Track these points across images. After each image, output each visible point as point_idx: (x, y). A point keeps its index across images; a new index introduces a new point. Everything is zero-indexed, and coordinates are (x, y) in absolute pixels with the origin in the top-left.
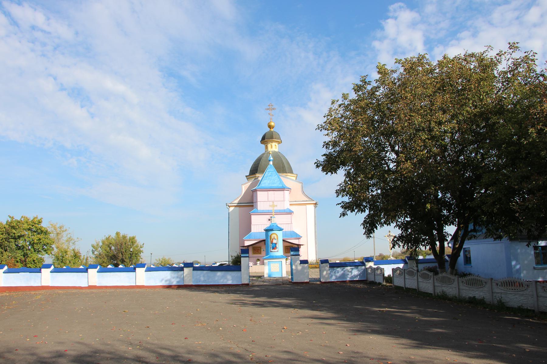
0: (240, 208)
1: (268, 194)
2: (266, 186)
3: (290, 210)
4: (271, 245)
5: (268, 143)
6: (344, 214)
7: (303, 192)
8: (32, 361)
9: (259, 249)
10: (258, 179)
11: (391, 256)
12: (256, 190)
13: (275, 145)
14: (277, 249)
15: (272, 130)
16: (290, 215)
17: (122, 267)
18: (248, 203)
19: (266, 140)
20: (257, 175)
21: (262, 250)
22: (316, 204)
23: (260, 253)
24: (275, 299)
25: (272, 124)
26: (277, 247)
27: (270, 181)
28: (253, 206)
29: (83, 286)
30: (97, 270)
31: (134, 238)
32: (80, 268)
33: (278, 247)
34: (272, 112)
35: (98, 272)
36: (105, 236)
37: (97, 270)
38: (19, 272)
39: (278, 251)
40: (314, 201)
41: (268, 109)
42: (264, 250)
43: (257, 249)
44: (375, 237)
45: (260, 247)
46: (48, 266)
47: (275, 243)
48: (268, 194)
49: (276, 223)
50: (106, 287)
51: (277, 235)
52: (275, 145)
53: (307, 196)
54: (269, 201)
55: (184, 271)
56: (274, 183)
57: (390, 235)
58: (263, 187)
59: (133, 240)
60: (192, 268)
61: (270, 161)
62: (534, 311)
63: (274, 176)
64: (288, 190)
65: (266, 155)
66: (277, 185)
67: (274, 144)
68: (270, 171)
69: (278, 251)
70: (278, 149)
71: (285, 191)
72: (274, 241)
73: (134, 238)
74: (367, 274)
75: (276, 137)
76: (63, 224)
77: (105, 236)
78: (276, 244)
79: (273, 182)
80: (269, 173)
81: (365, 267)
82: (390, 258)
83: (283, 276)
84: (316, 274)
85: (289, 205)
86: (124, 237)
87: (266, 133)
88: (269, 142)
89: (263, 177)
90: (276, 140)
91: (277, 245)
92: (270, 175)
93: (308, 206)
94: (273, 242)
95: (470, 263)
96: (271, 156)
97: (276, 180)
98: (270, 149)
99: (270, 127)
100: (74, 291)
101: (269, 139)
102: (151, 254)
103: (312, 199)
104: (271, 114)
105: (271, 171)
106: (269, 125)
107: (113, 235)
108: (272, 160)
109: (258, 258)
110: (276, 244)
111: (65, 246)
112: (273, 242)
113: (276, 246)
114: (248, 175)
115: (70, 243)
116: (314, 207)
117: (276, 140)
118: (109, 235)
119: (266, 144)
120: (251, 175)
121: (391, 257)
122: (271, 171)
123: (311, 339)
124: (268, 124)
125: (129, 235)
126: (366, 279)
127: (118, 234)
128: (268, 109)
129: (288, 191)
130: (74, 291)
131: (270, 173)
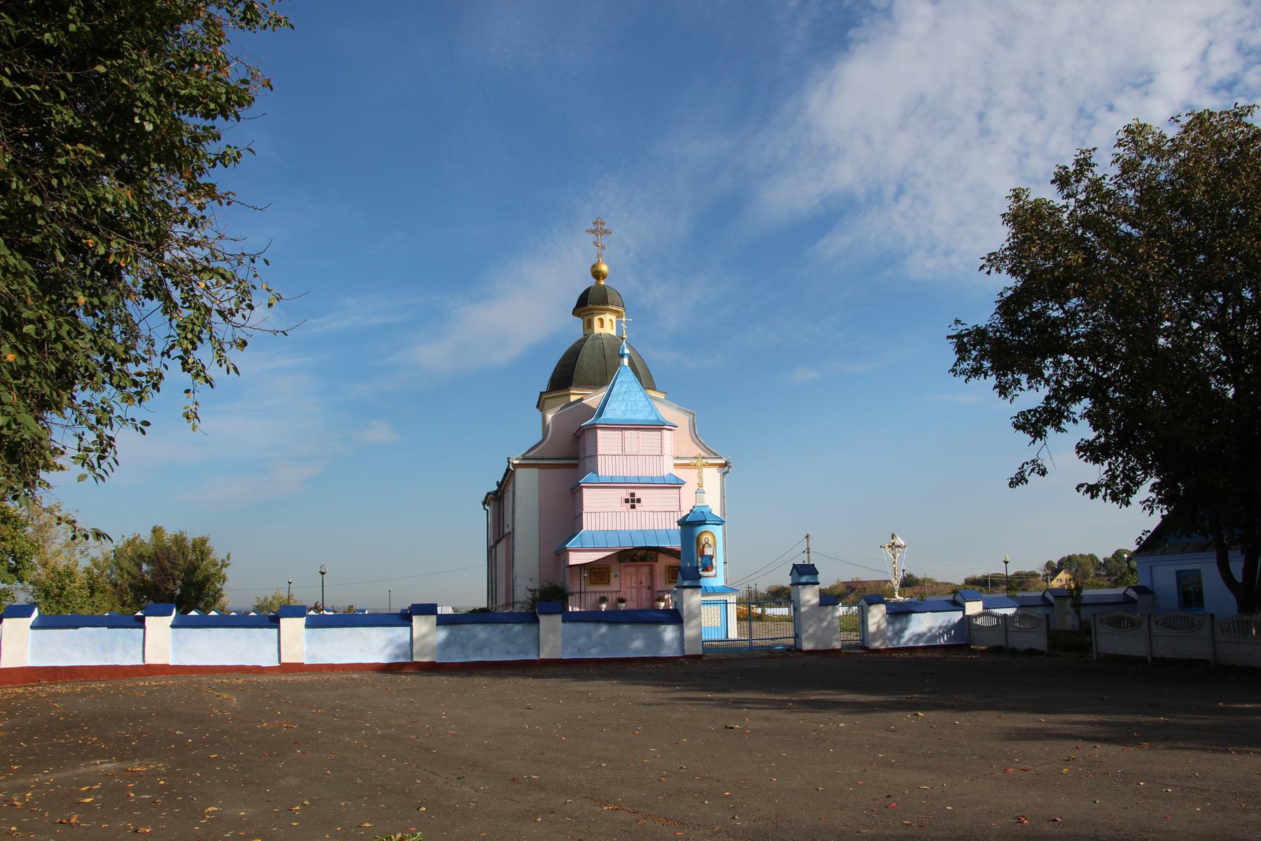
0: (541, 470)
1: (623, 437)
2: (618, 418)
3: (677, 479)
4: (700, 559)
5: (593, 314)
7: (694, 435)
10: (583, 402)
11: (897, 593)
12: (594, 426)
13: (611, 320)
15: (602, 283)
16: (677, 491)
17: (196, 614)
18: (562, 459)
19: (590, 306)
20: (571, 392)
21: (612, 574)
22: (725, 465)
23: (608, 583)
24: (825, 694)
25: (604, 268)
26: (714, 564)
27: (627, 405)
28: (576, 466)
29: (264, 664)
30: (30, 621)
31: (203, 541)
32: (210, 614)
34: (604, 240)
35: (32, 627)
36: (123, 536)
37: (30, 621)
38: (76, 627)
39: (715, 576)
40: (721, 458)
41: (593, 232)
42: (616, 576)
44: (811, 550)
46: (23, 612)
47: (711, 556)
48: (623, 437)
49: (707, 506)
50: (332, 668)
51: (713, 535)
52: (611, 320)
53: (705, 446)
55: (541, 624)
56: (636, 411)
57: (893, 544)
58: (612, 420)
59: (201, 547)
60: (434, 618)
61: (622, 356)
63: (636, 394)
64: (671, 430)
65: (590, 342)
66: (643, 416)
67: (608, 317)
68: (624, 382)
69: (715, 576)
70: (617, 330)
71: (665, 431)
72: (708, 551)
73: (203, 541)
74: (970, 629)
75: (613, 302)
76: (59, 501)
77: (123, 536)
78: (711, 557)
79: (634, 408)
80: (621, 387)
81: (964, 612)
82: (895, 598)
83: (729, 637)
84: (776, 631)
85: (672, 465)
86: (179, 541)
87: (588, 289)
89: (609, 395)
90: (614, 308)
91: (714, 560)
92: (626, 392)
93: (706, 471)
95: (1202, 606)
96: (624, 343)
97: (641, 405)
98: (597, 329)
99: (597, 275)
100: (335, 677)
101: (599, 304)
102: (290, 583)
103: (716, 454)
104: (600, 245)
105: (627, 382)
106: (595, 269)
107: (146, 537)
108: (627, 355)
109: (602, 595)
110: (711, 557)
111: (62, 563)
112: (705, 554)
113: (712, 563)
114: (545, 390)
115: (76, 552)
116: (718, 475)
117: (614, 308)
118: (135, 534)
119: (586, 318)
120: (552, 391)
121: (896, 596)
122: (627, 382)
123: (887, 795)
124: (594, 266)
125: (192, 535)
126: (965, 642)
127: (156, 531)
129: (669, 432)
130: (335, 677)
131: (625, 386)
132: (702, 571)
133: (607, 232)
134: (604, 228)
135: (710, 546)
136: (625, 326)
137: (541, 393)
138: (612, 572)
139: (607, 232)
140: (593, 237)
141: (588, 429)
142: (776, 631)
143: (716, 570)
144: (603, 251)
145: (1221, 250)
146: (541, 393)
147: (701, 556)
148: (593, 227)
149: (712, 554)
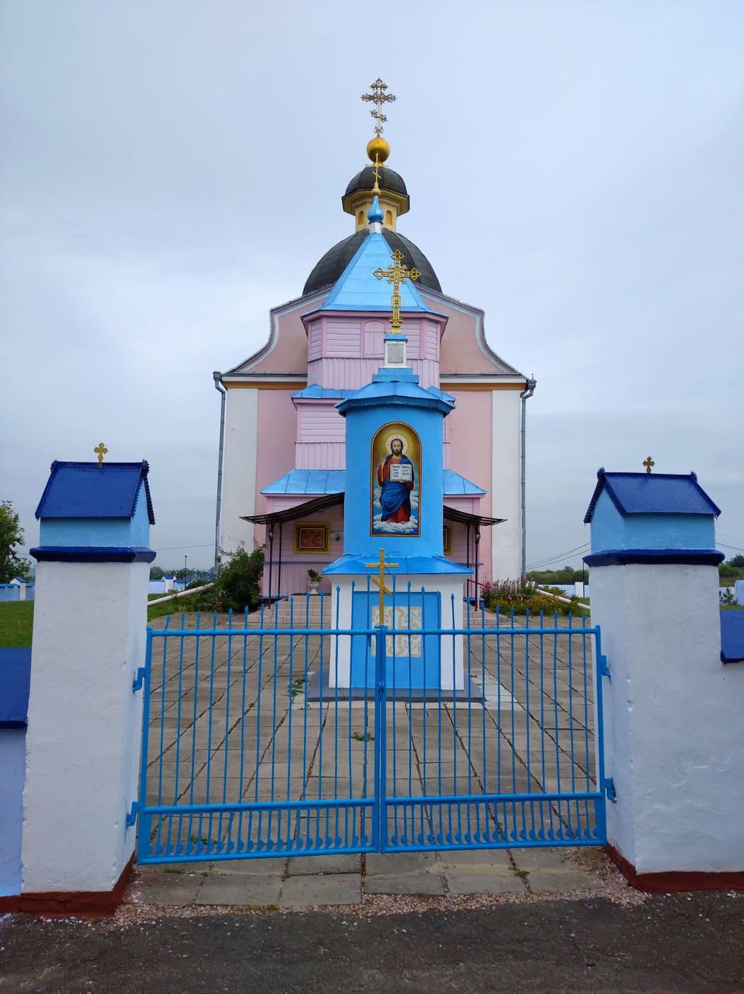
5: (365, 203)
6: (649, 463)
8: (73, 918)
9: (319, 534)
14: (412, 518)
23: (325, 548)
26: (414, 504)
33: (418, 509)
34: (385, 108)
39: (416, 532)
41: (371, 98)
43: (312, 532)
45: (323, 526)
54: (366, 356)
62: (21, 843)
64: (437, 322)
69: (416, 532)
78: (407, 487)
88: (367, 200)
91: (413, 494)
93: (497, 394)
94: (393, 478)
112: (393, 478)
128: (371, 98)
132: (383, 519)
133: (390, 98)
134: (386, 93)
135: (404, 460)
136: (376, 174)
137: (691, 478)
138: (332, 532)
139: (390, 98)
140: (371, 105)
141: (328, 317)
142: (563, 673)
143: (418, 518)
144: (384, 124)
145: (422, 917)
146: (691, 478)
147: (382, 484)
148: (371, 92)
149: (408, 478)
